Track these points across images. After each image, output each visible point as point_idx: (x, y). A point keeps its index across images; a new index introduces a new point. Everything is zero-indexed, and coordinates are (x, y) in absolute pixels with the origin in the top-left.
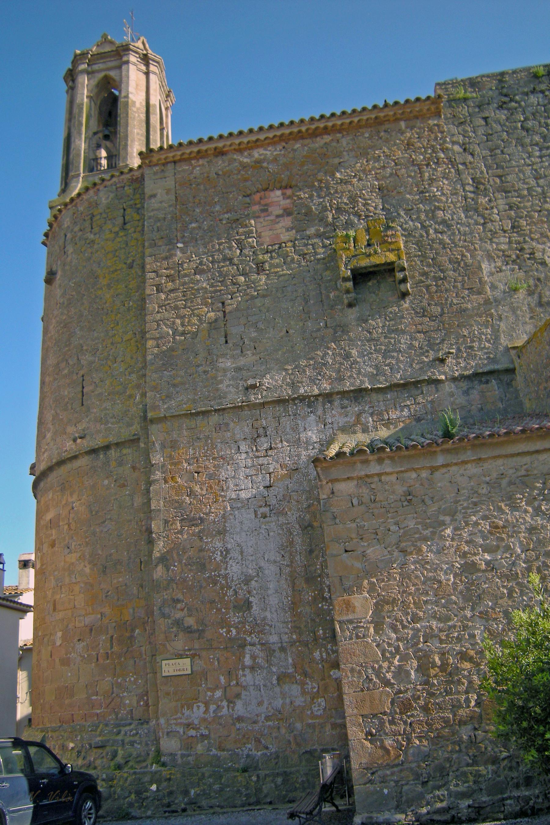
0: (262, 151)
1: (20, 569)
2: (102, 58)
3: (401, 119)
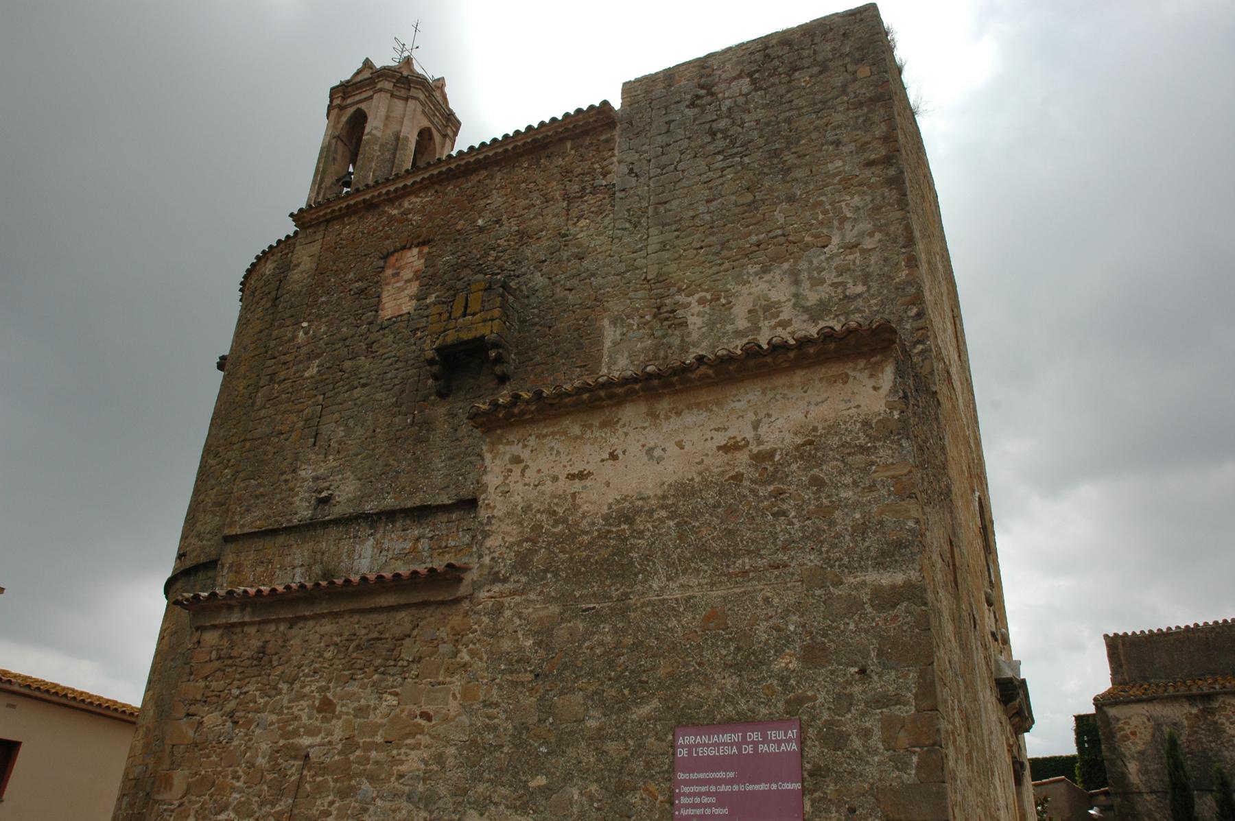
0: (414, 199)
1: (1095, 699)
2: (358, 89)
3: (567, 138)
